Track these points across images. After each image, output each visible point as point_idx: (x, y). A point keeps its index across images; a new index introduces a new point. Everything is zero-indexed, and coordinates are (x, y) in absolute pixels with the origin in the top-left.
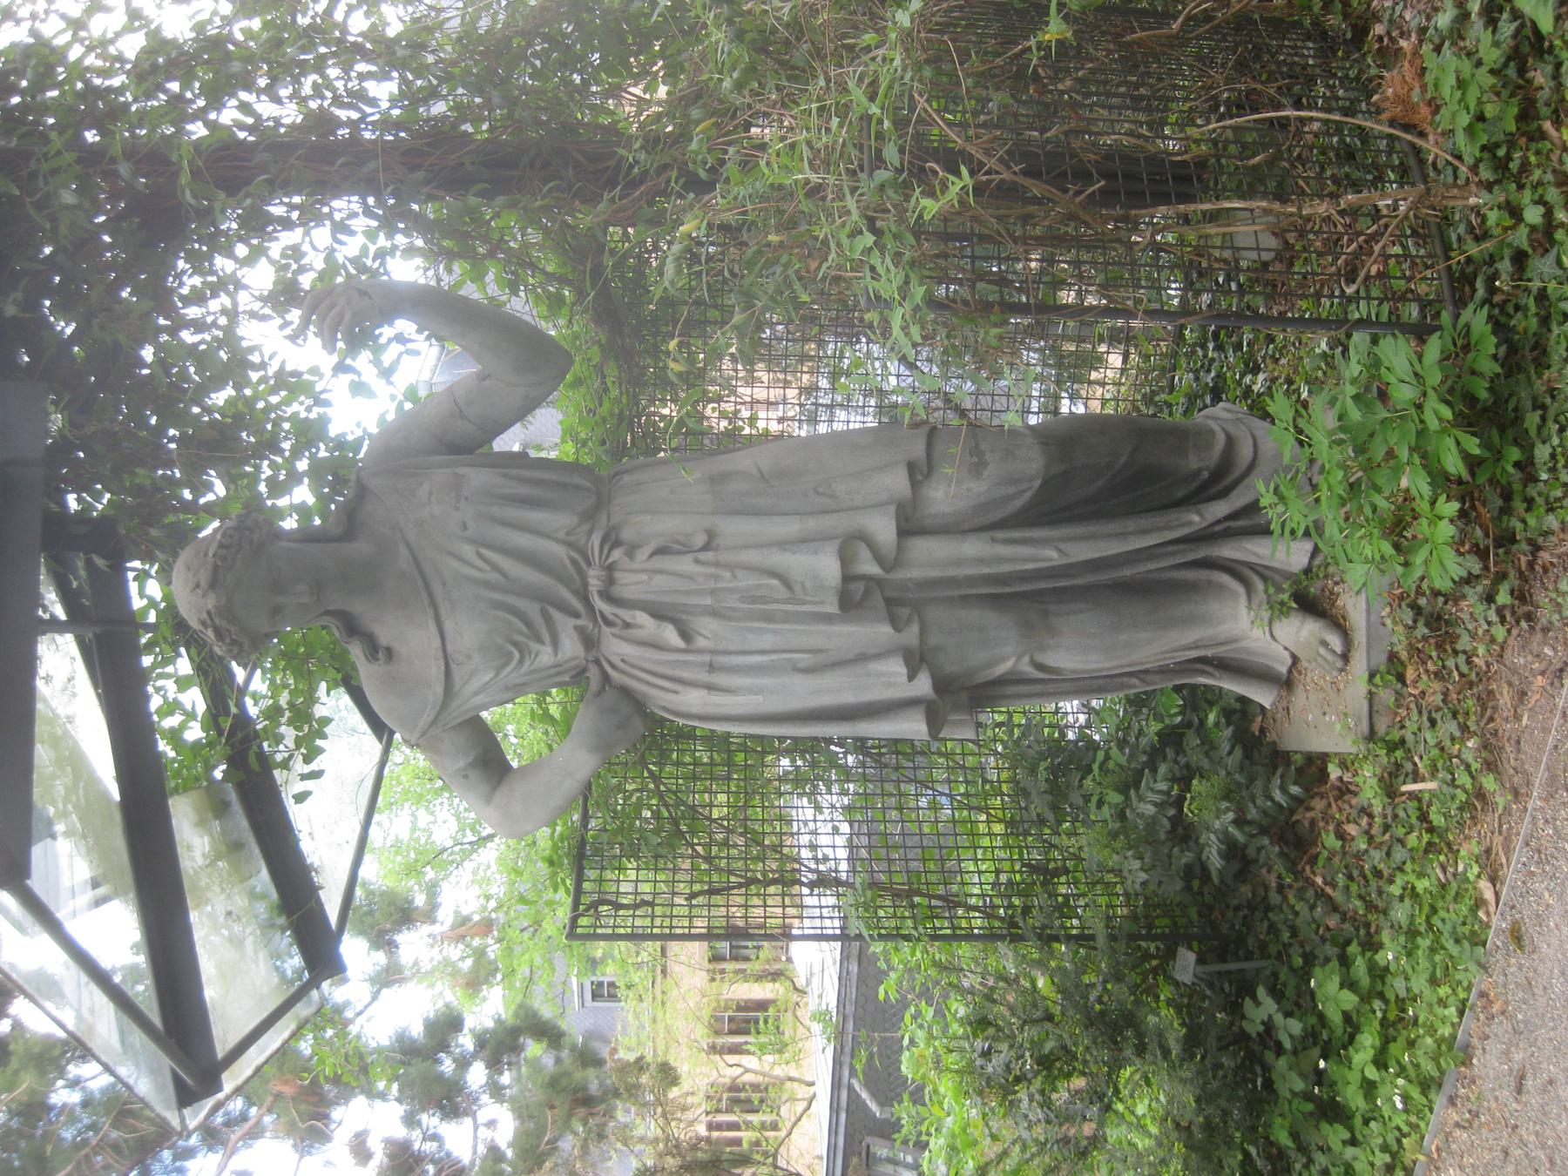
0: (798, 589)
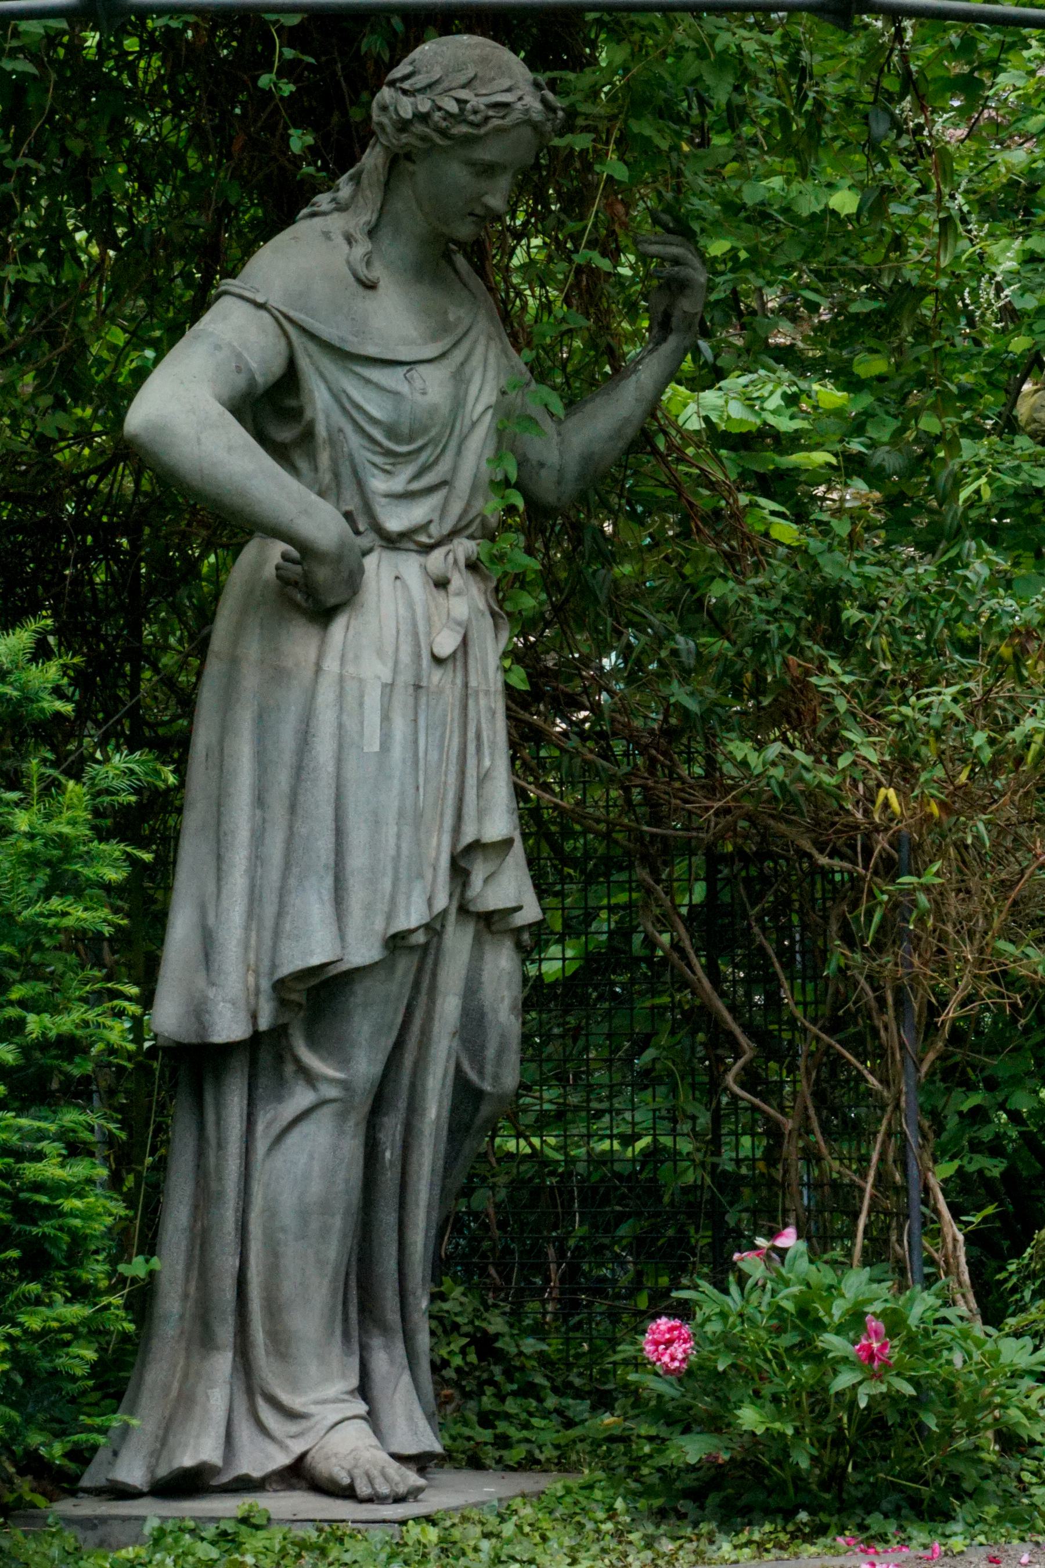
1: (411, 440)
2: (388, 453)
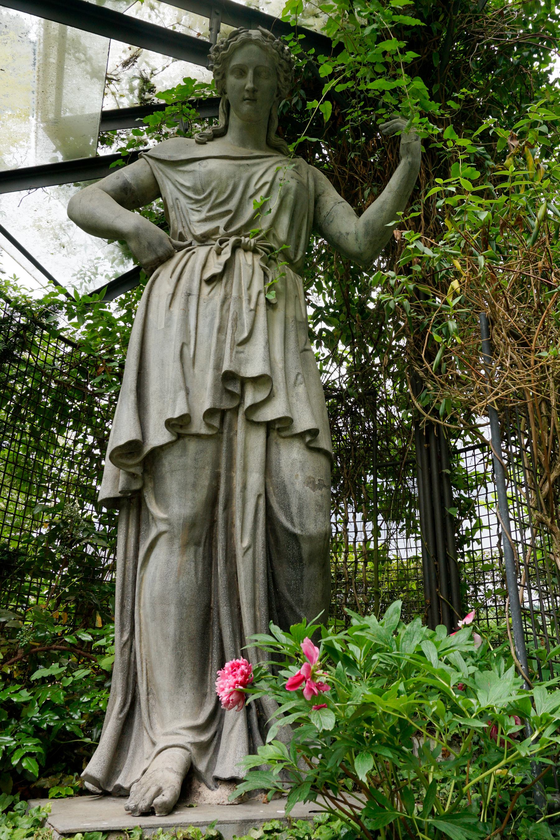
0: (240, 349)
1: (204, 191)
2: (197, 201)
